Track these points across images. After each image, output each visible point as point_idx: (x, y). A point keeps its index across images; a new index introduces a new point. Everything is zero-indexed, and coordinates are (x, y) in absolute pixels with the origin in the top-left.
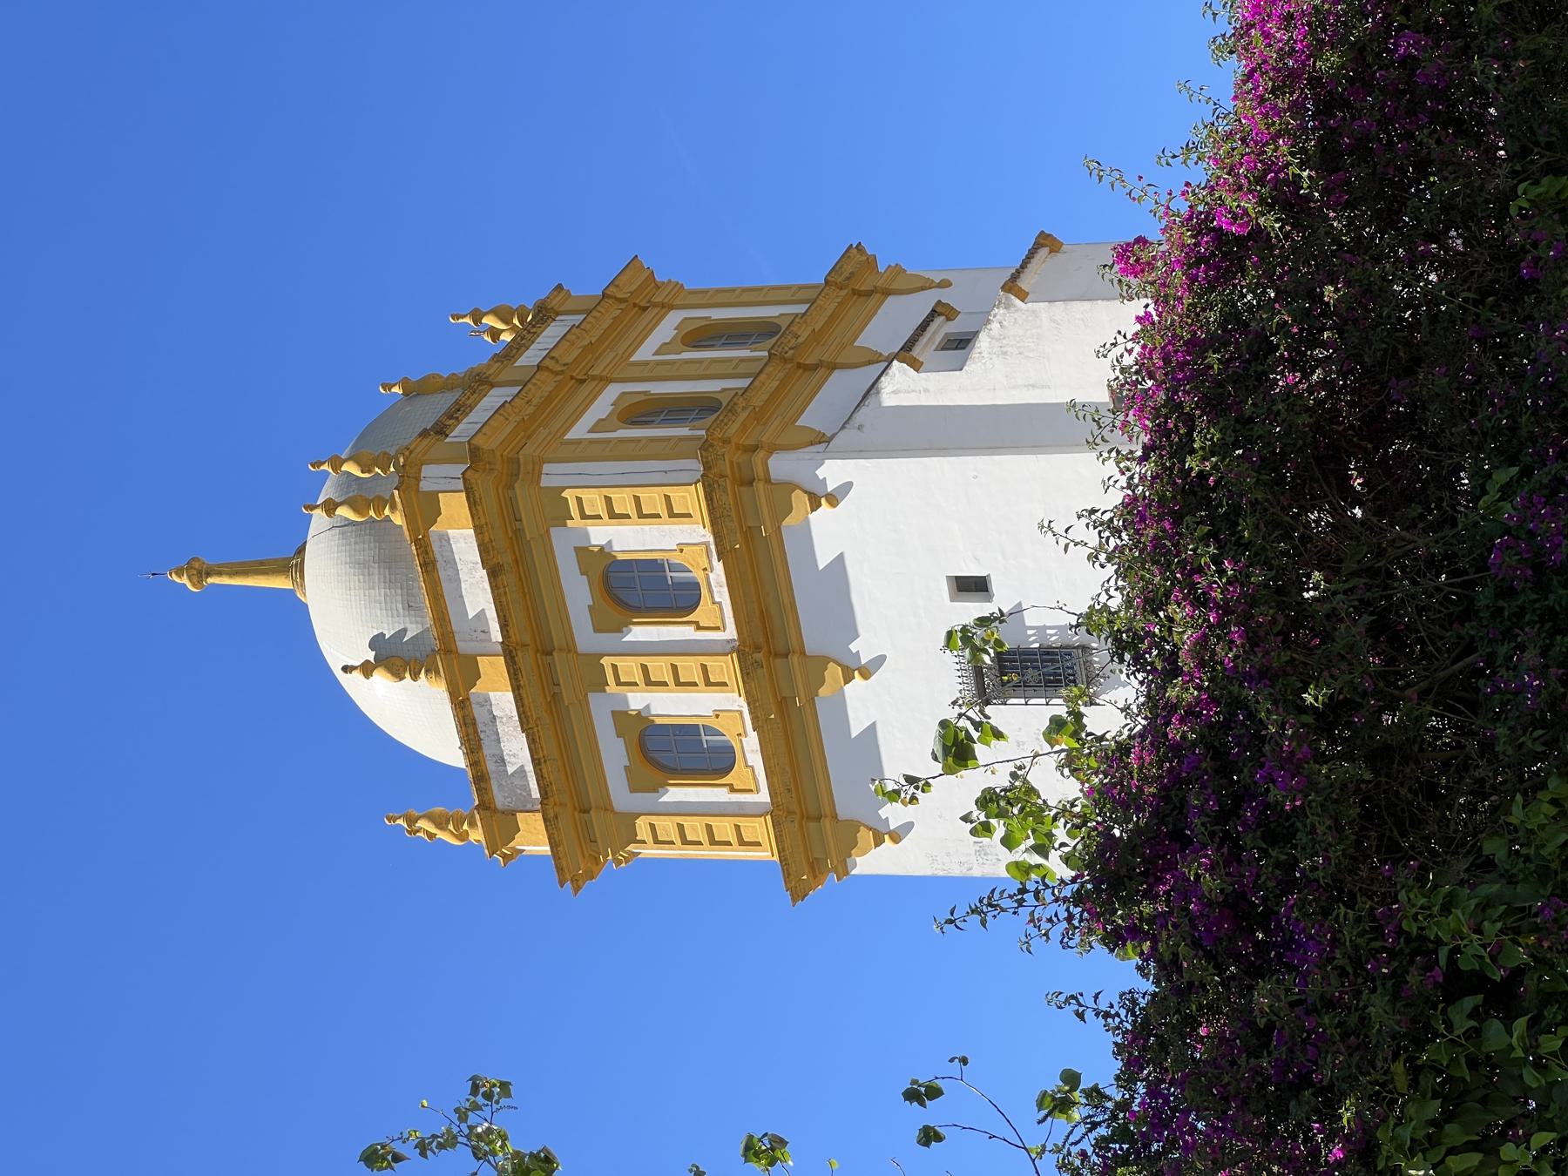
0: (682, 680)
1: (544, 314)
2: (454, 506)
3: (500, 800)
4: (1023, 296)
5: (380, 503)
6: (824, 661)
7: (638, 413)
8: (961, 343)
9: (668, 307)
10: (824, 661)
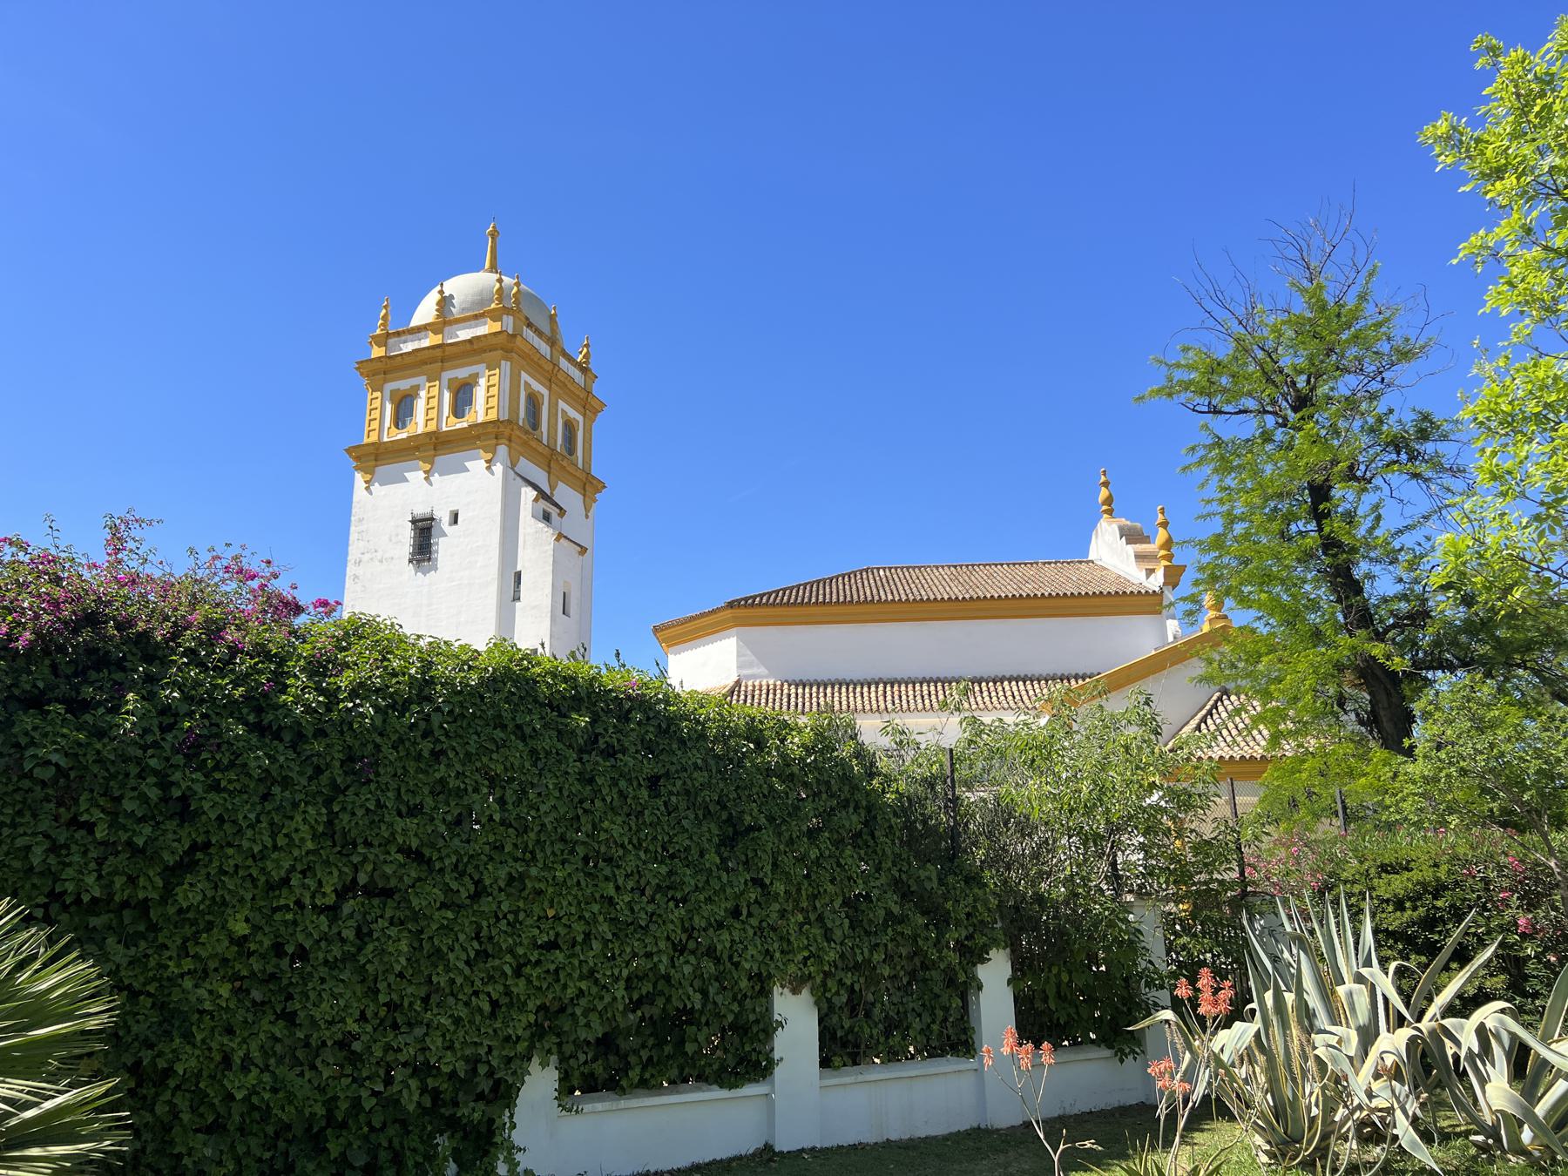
0: (430, 410)
1: (584, 370)
2: (496, 327)
3: (391, 341)
4: (557, 539)
5: (500, 300)
6: (432, 464)
7: (533, 401)
8: (547, 517)
9: (584, 416)
10: (432, 464)
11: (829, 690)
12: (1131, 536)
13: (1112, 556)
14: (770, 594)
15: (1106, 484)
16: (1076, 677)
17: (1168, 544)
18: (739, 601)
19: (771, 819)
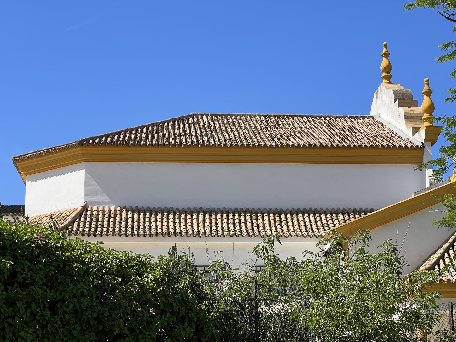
11: (159, 216)
12: (403, 99)
13: (388, 115)
14: (113, 135)
15: (386, 55)
16: (354, 212)
17: (431, 109)
18: (88, 140)
19: (132, 330)
